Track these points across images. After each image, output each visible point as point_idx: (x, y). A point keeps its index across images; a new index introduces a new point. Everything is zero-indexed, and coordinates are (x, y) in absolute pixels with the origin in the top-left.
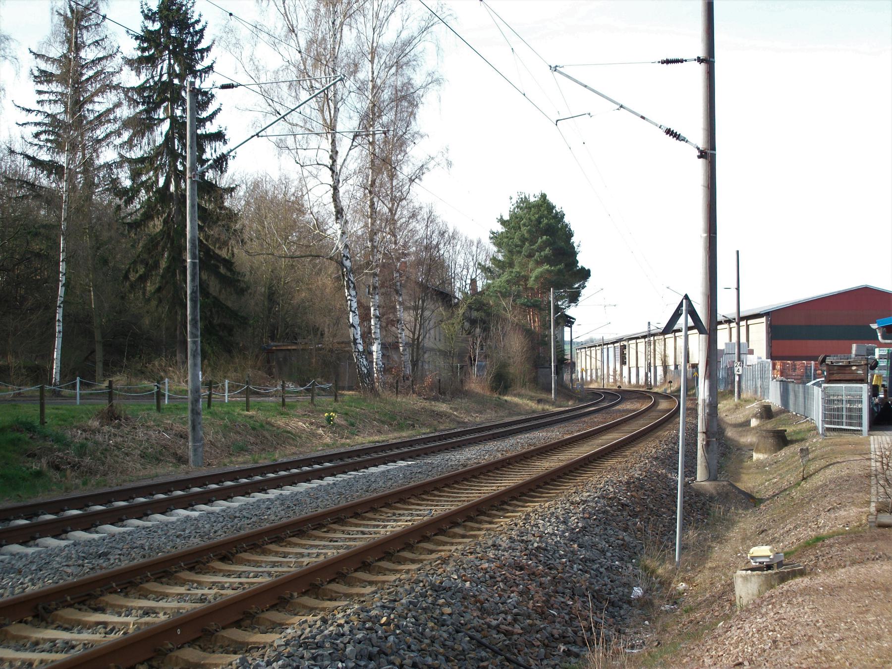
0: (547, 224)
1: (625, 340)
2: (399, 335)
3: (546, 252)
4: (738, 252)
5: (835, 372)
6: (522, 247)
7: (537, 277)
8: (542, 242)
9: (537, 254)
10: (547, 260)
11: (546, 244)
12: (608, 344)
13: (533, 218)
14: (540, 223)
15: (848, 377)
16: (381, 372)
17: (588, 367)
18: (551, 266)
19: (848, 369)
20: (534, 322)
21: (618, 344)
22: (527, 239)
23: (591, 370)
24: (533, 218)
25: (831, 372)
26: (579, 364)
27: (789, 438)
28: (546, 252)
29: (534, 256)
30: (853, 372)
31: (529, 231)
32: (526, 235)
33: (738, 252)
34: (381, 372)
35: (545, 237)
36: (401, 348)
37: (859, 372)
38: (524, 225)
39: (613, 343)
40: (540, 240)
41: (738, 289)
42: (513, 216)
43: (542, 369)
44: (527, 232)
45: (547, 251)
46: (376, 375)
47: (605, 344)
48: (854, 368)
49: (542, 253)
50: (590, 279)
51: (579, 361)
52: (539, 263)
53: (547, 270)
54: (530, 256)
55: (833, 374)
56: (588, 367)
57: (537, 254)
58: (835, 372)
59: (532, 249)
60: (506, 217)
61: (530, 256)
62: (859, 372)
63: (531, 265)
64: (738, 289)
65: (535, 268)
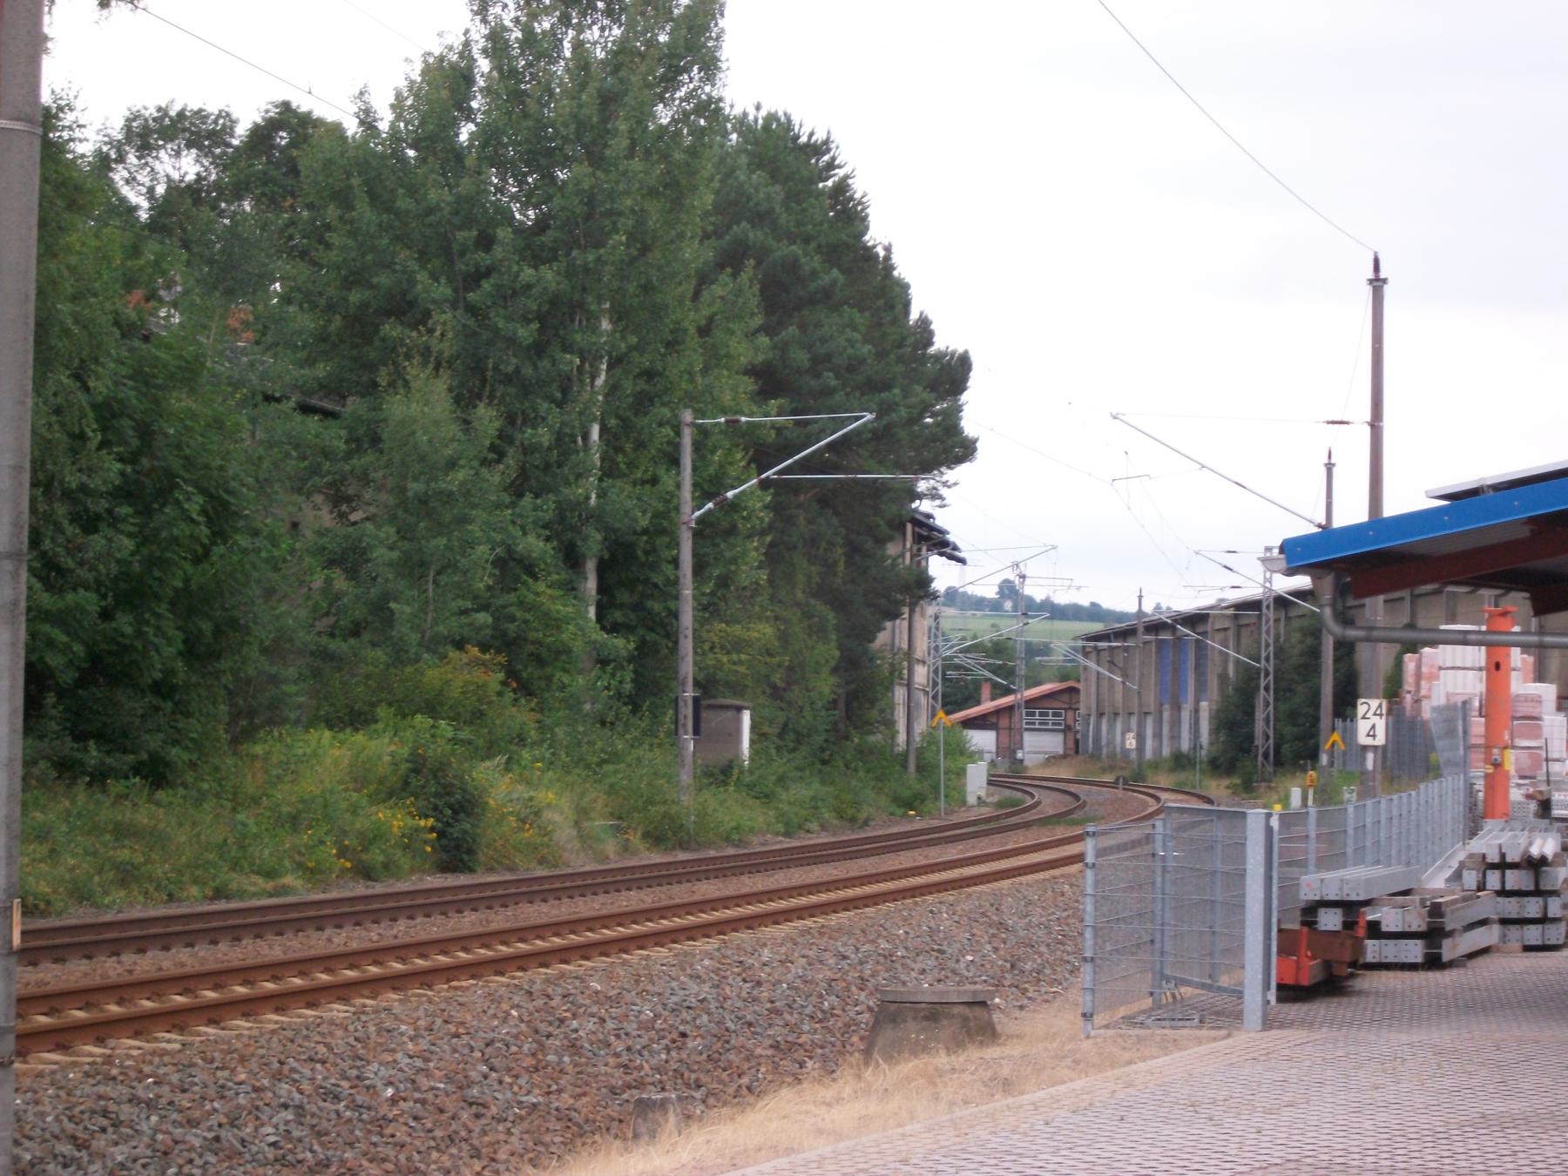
4: (1328, 423)
33: (1328, 423)
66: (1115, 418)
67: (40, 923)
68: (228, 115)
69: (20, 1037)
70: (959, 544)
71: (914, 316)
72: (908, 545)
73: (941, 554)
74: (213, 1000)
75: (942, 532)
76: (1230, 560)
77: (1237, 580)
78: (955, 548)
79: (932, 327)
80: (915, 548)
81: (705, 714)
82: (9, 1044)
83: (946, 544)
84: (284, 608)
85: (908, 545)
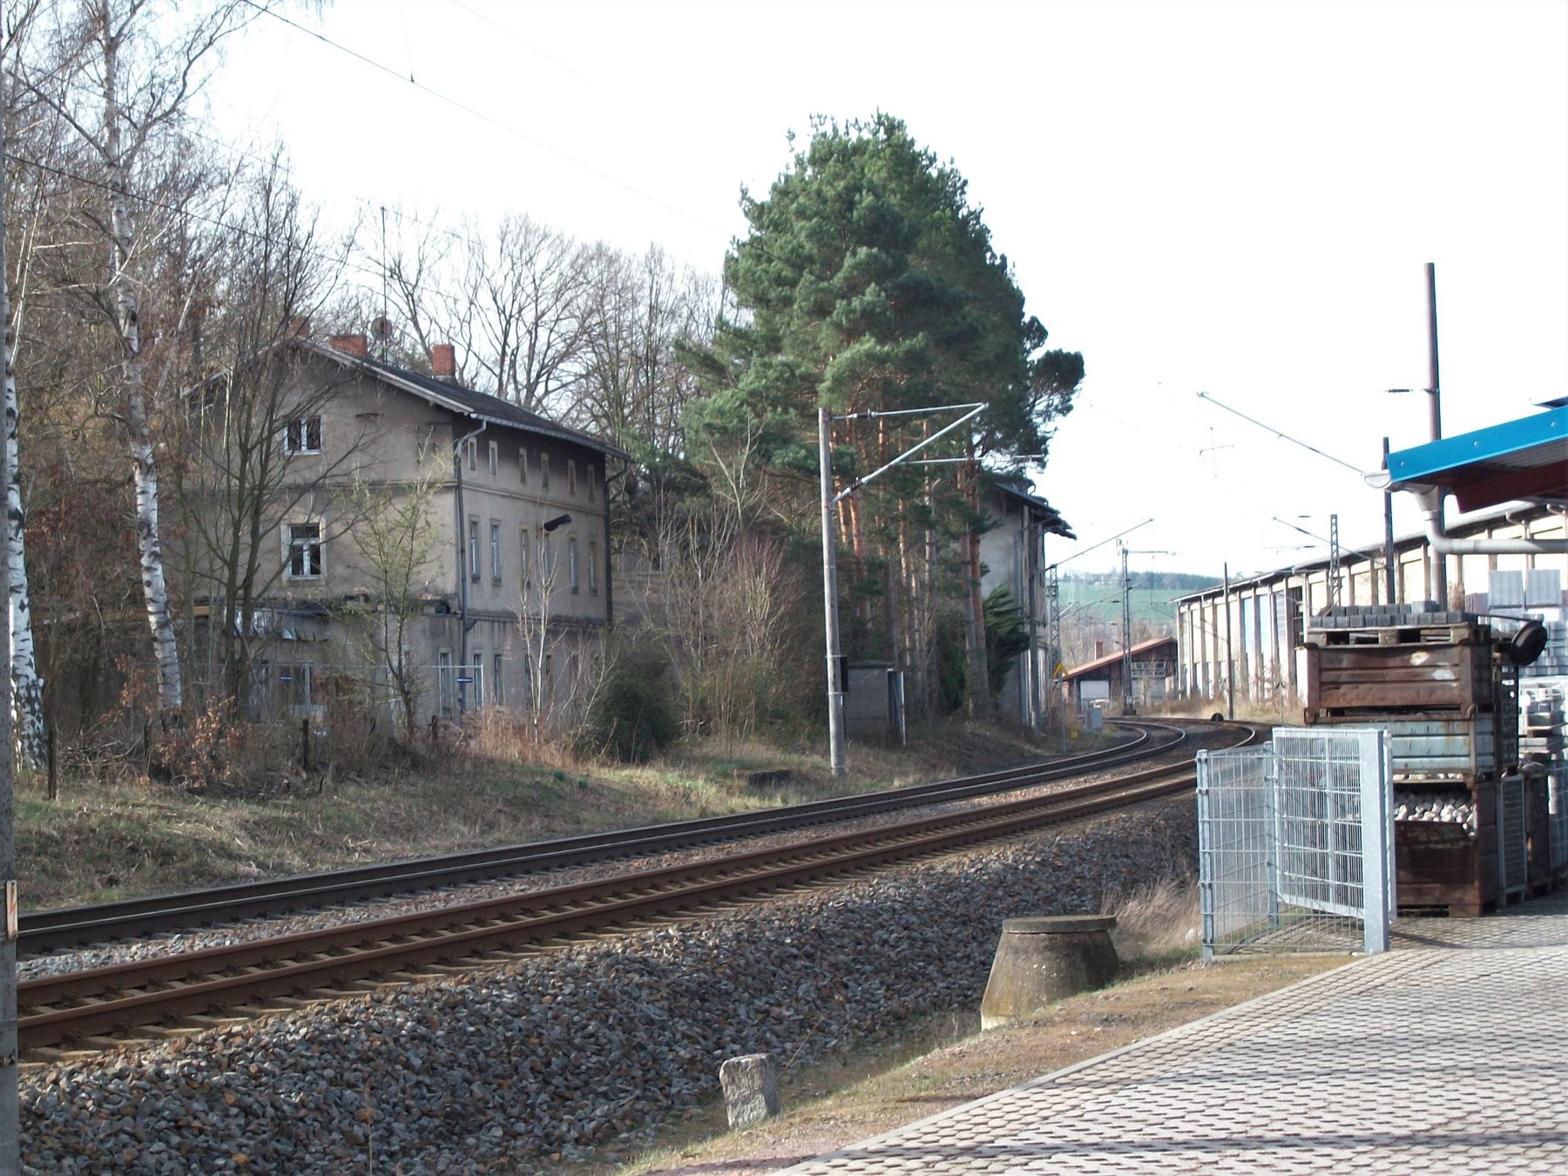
0: (872, 209)
1: (1298, 574)
2: (146, 577)
3: (868, 298)
4: (1431, 269)
5: (1344, 676)
6: (793, 284)
7: (838, 381)
8: (854, 267)
9: (840, 304)
10: (868, 322)
11: (872, 272)
12: (1254, 586)
13: (830, 192)
14: (851, 205)
15: (1396, 696)
16: (30, 700)
17: (1210, 658)
18: (881, 342)
19: (1396, 661)
20: (847, 522)
21: (1279, 587)
22: (810, 259)
23: (1218, 664)
24: (830, 192)
25: (1327, 676)
26: (1187, 648)
27: (1124, 951)
28: (868, 298)
29: (830, 313)
30: (1415, 677)
31: (813, 234)
32: (809, 247)
33: (1431, 269)
34: (30, 700)
35: (863, 251)
36: (152, 619)
37: (1439, 674)
38: (802, 214)
39: (1270, 581)
40: (848, 261)
41: (1434, 391)
42: (783, 192)
43: (861, 673)
44: (810, 236)
45: (871, 293)
46: (14, 713)
47: (1234, 590)
48: (1419, 658)
49: (856, 303)
50: (1083, 385)
51: (1187, 636)
52: (851, 334)
53: (870, 356)
54: (821, 310)
55: (1336, 685)
56: (1210, 658)
57: (840, 304)
58: (1344, 676)
59: (823, 290)
60: (762, 195)
61: (821, 310)
62: (1439, 674)
63: (825, 334)
64: (1434, 391)
65: (839, 349)
66: (1202, 395)
67: (41, 909)
68: (600, 251)
69: (24, 1030)
70: (1069, 523)
71: (1026, 319)
72: (1026, 524)
73: (1055, 532)
74: (294, 969)
75: (1056, 512)
76: (1303, 524)
77: (1308, 540)
78: (1067, 526)
79: (1065, 351)
80: (1032, 526)
81: (852, 674)
82: (12, 1041)
83: (1059, 522)
84: (119, 570)
85: (1026, 524)
